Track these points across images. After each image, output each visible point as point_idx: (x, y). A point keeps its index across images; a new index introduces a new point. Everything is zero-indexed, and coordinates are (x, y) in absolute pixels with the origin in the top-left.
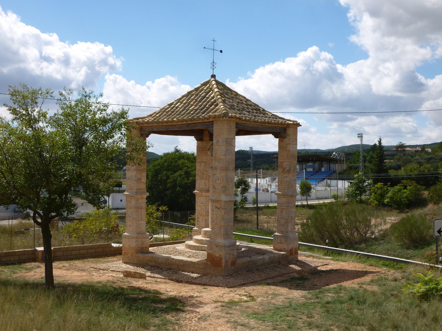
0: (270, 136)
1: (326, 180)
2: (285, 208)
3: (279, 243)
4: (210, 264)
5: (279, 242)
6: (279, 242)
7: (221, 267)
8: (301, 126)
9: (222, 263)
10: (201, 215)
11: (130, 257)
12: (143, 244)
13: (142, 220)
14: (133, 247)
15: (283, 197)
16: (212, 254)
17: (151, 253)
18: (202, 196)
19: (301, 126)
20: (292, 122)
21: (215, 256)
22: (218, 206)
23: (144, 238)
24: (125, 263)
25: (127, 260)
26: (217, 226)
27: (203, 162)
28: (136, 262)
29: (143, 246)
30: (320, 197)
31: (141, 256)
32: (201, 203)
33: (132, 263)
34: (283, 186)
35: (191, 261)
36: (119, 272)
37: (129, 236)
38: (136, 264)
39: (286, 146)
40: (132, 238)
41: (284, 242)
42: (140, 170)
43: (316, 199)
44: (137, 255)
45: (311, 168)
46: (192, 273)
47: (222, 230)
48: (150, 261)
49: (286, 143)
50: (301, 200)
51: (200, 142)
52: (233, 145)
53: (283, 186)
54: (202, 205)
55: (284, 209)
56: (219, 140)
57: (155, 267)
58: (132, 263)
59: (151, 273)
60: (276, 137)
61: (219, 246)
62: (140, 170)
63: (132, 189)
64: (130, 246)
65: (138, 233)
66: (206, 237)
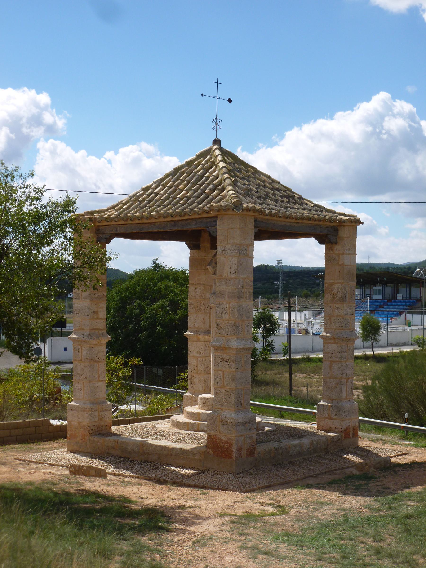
0: (312, 241)
1: (403, 315)
2: (336, 360)
3: (327, 418)
4: (211, 452)
5: (327, 416)
6: (327, 416)
7: (231, 458)
8: (362, 223)
9: (232, 451)
10: (197, 373)
11: (80, 441)
12: (101, 420)
13: (99, 381)
14: (84, 426)
15: (332, 341)
16: (215, 437)
17: (115, 434)
18: (198, 340)
19: (362, 223)
20: (347, 218)
21: (221, 440)
22: (225, 356)
23: (103, 411)
24: (71, 452)
25: (75, 447)
26: (224, 390)
27: (200, 284)
28: (89, 450)
29: (102, 424)
30: (395, 342)
31: (98, 439)
32: (197, 353)
33: (84, 452)
34: (333, 324)
35: (181, 449)
36: (62, 466)
37: (78, 407)
38: (90, 453)
39: (337, 258)
40: (84, 410)
41: (335, 417)
42: (96, 298)
43: (388, 346)
44: (92, 439)
45: (379, 294)
46: (183, 468)
47: (233, 396)
48: (113, 448)
49: (337, 252)
50: (364, 348)
51: (195, 251)
52: (250, 255)
53: (333, 324)
54: (198, 355)
55: (334, 362)
56: (227, 247)
57: (121, 457)
58: (84, 452)
59: (115, 468)
60: (321, 242)
61: (227, 423)
62: (96, 298)
63: (83, 329)
64: (79, 423)
65: (93, 403)
66: (206, 408)
